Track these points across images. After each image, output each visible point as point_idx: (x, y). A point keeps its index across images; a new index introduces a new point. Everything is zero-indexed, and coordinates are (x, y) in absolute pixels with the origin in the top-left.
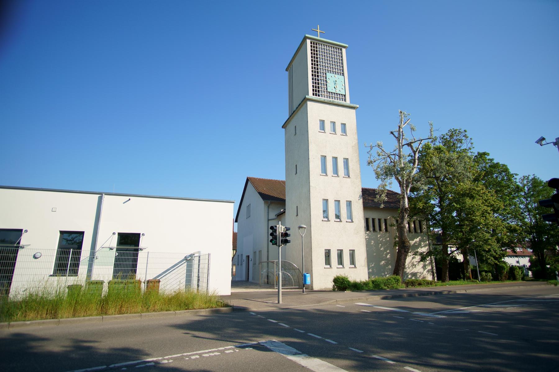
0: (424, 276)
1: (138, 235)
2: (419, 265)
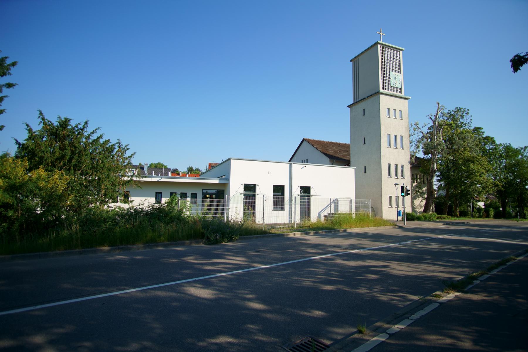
1: (255, 185)
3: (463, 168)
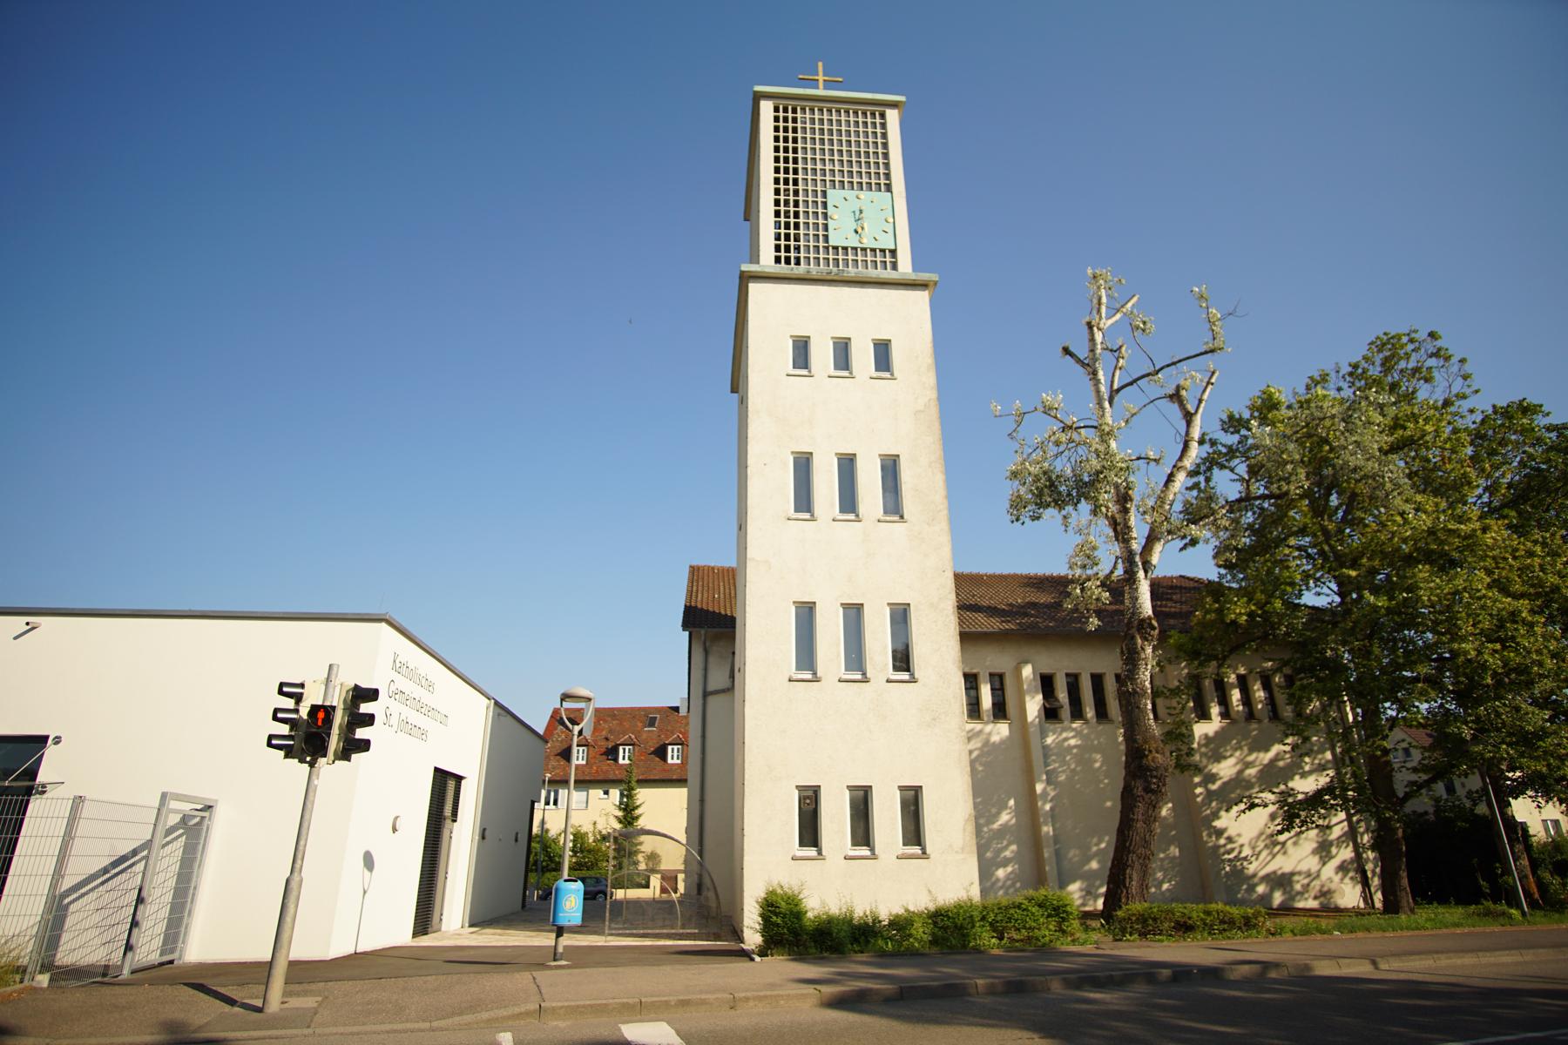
0: (1323, 886)
2: (1301, 842)
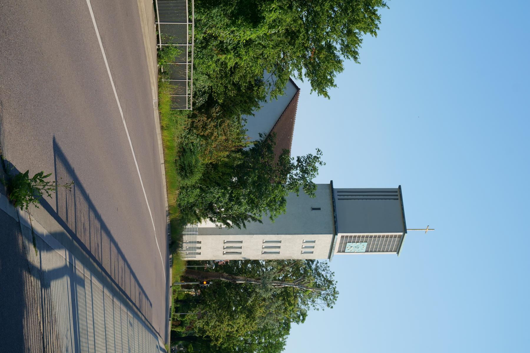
3: (240, 307)
